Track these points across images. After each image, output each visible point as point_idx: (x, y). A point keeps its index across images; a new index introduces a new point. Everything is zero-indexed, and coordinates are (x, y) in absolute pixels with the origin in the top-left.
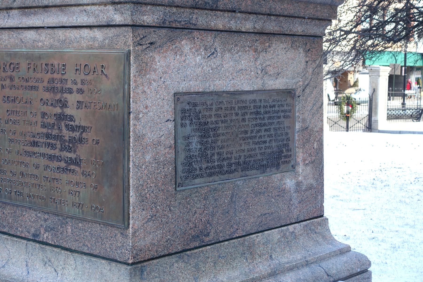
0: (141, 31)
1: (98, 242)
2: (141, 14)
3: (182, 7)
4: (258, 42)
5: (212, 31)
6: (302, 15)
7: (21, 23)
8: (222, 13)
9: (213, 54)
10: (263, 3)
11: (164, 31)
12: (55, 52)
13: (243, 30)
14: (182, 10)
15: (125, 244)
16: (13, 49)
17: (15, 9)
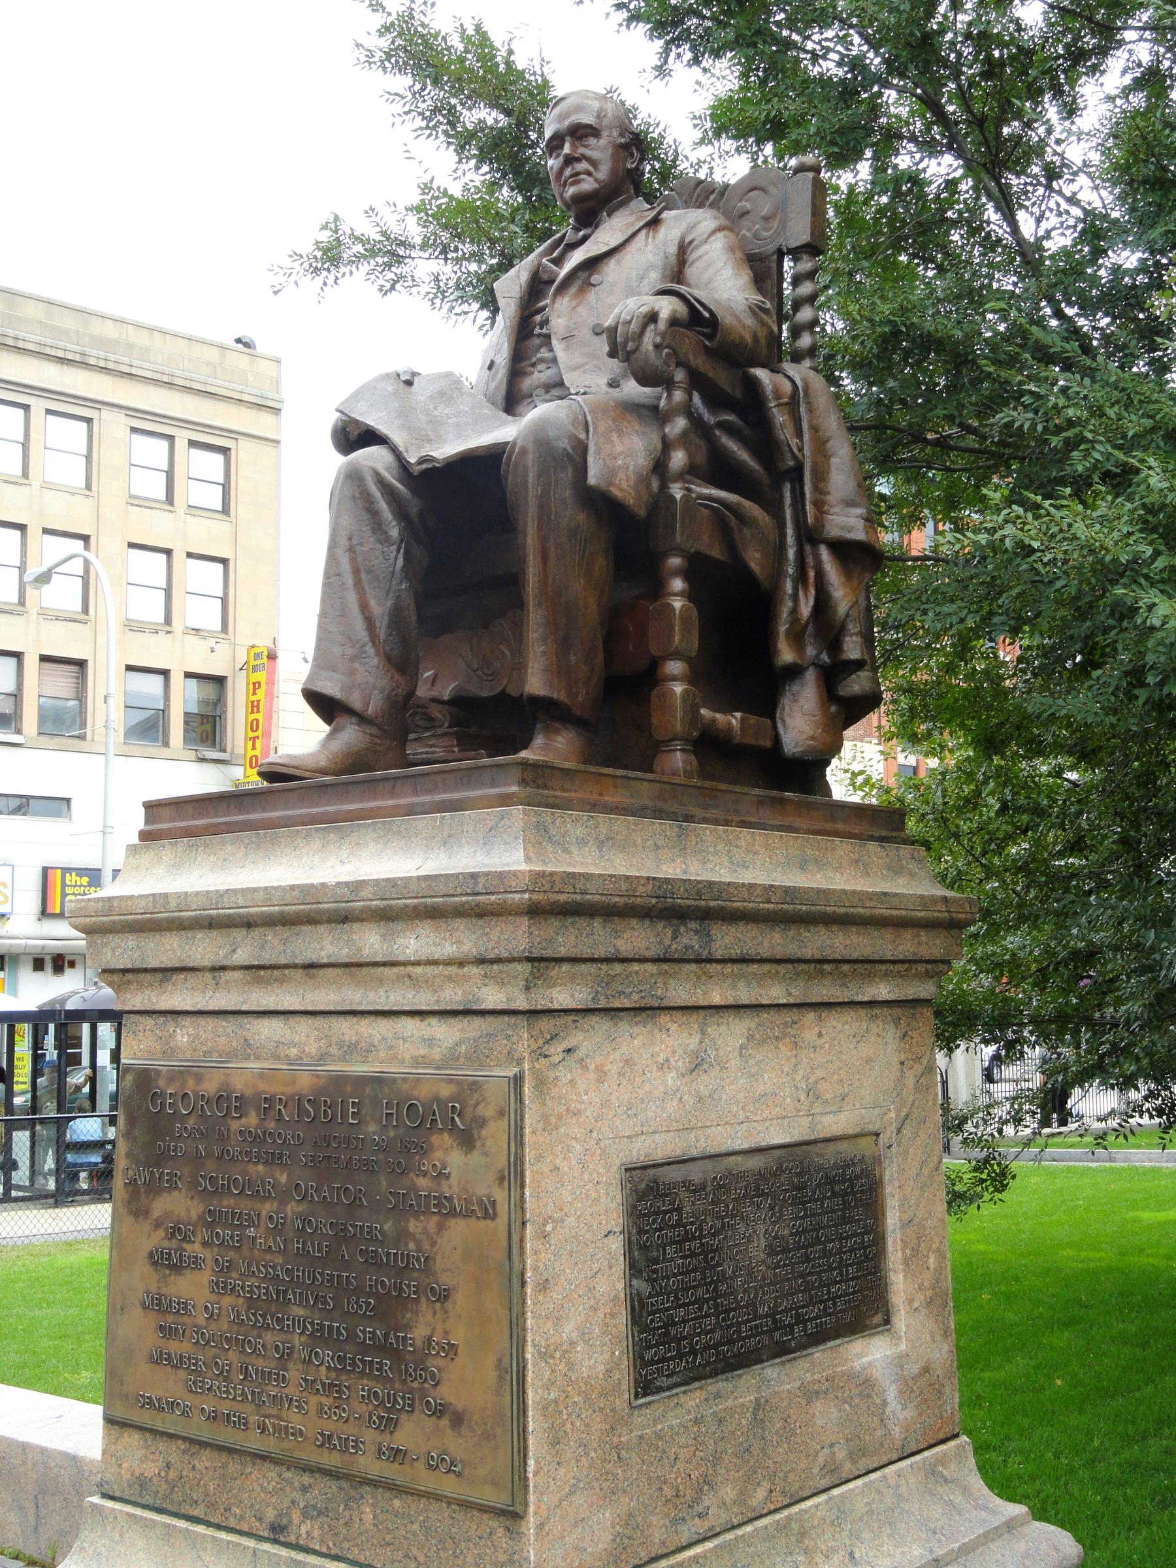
0: (545, 1025)
1: (445, 1549)
7: (245, 1002)
15: (516, 1557)
17: (233, 968)
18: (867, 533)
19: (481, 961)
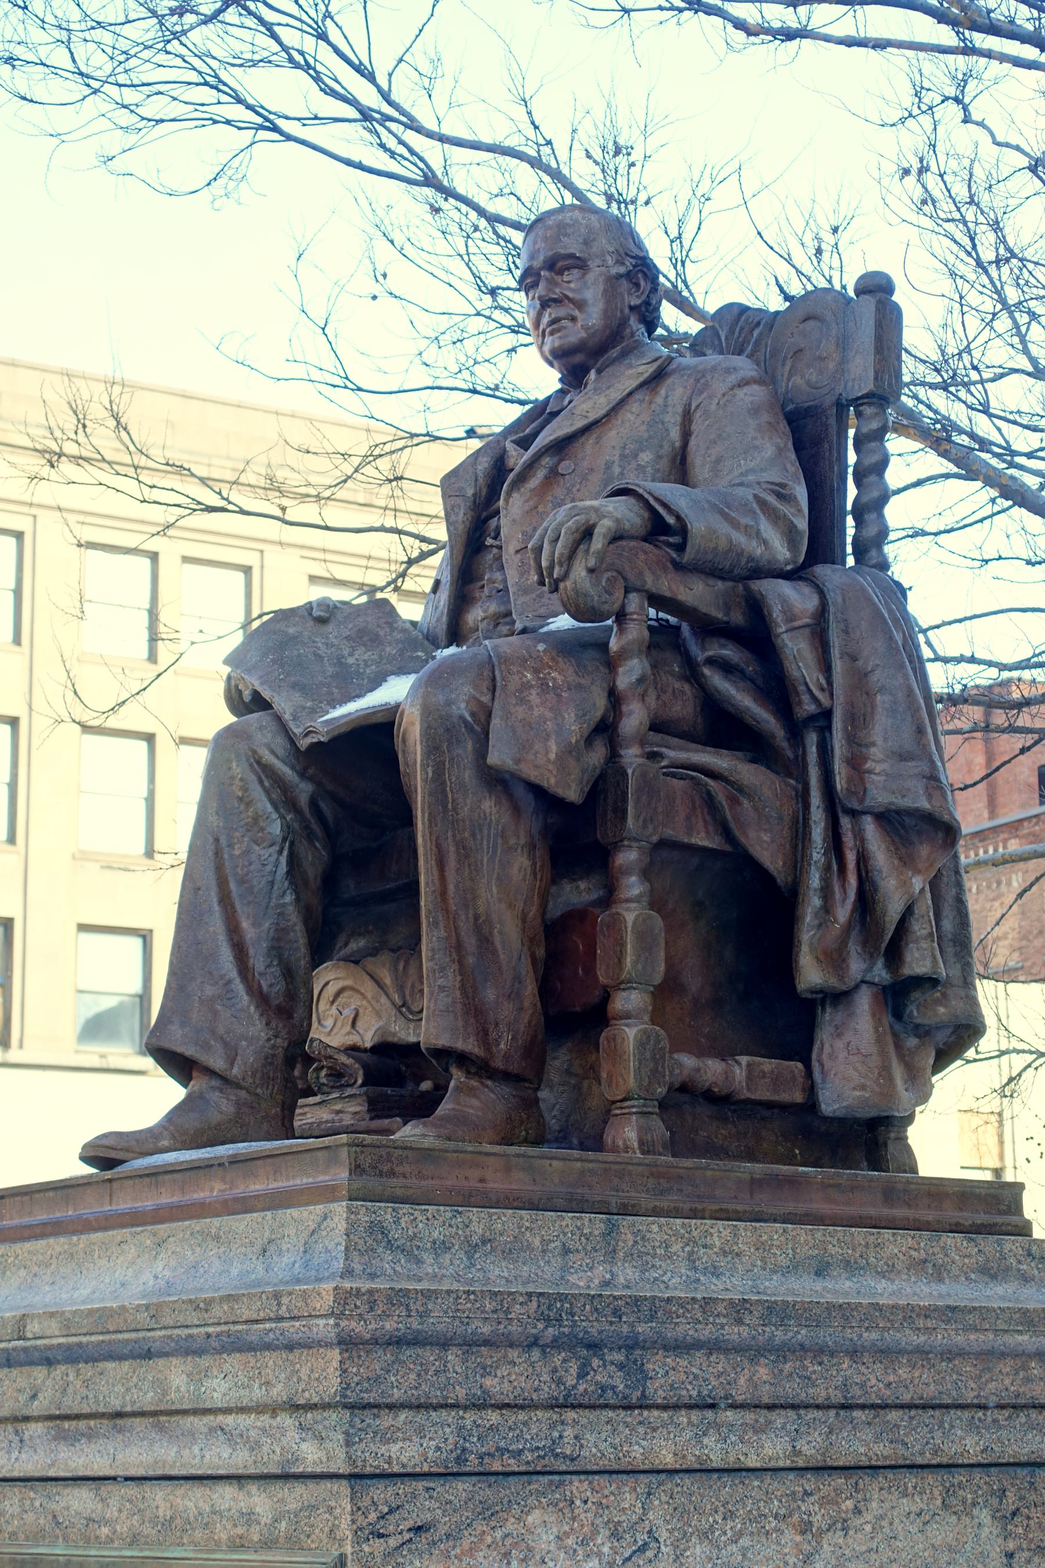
0: (381, 1493)
2: (378, 1439)
3: (522, 1407)
4: (812, 1499)
5: (637, 1476)
6: (970, 1397)
7: (53, 1465)
8: (665, 1415)
9: (643, 1548)
10: (814, 1372)
11: (462, 1487)
12: (143, 1557)
13: (752, 1462)
14: (522, 1416)
16: (32, 1547)
18: (930, 797)
19: (295, 1408)
